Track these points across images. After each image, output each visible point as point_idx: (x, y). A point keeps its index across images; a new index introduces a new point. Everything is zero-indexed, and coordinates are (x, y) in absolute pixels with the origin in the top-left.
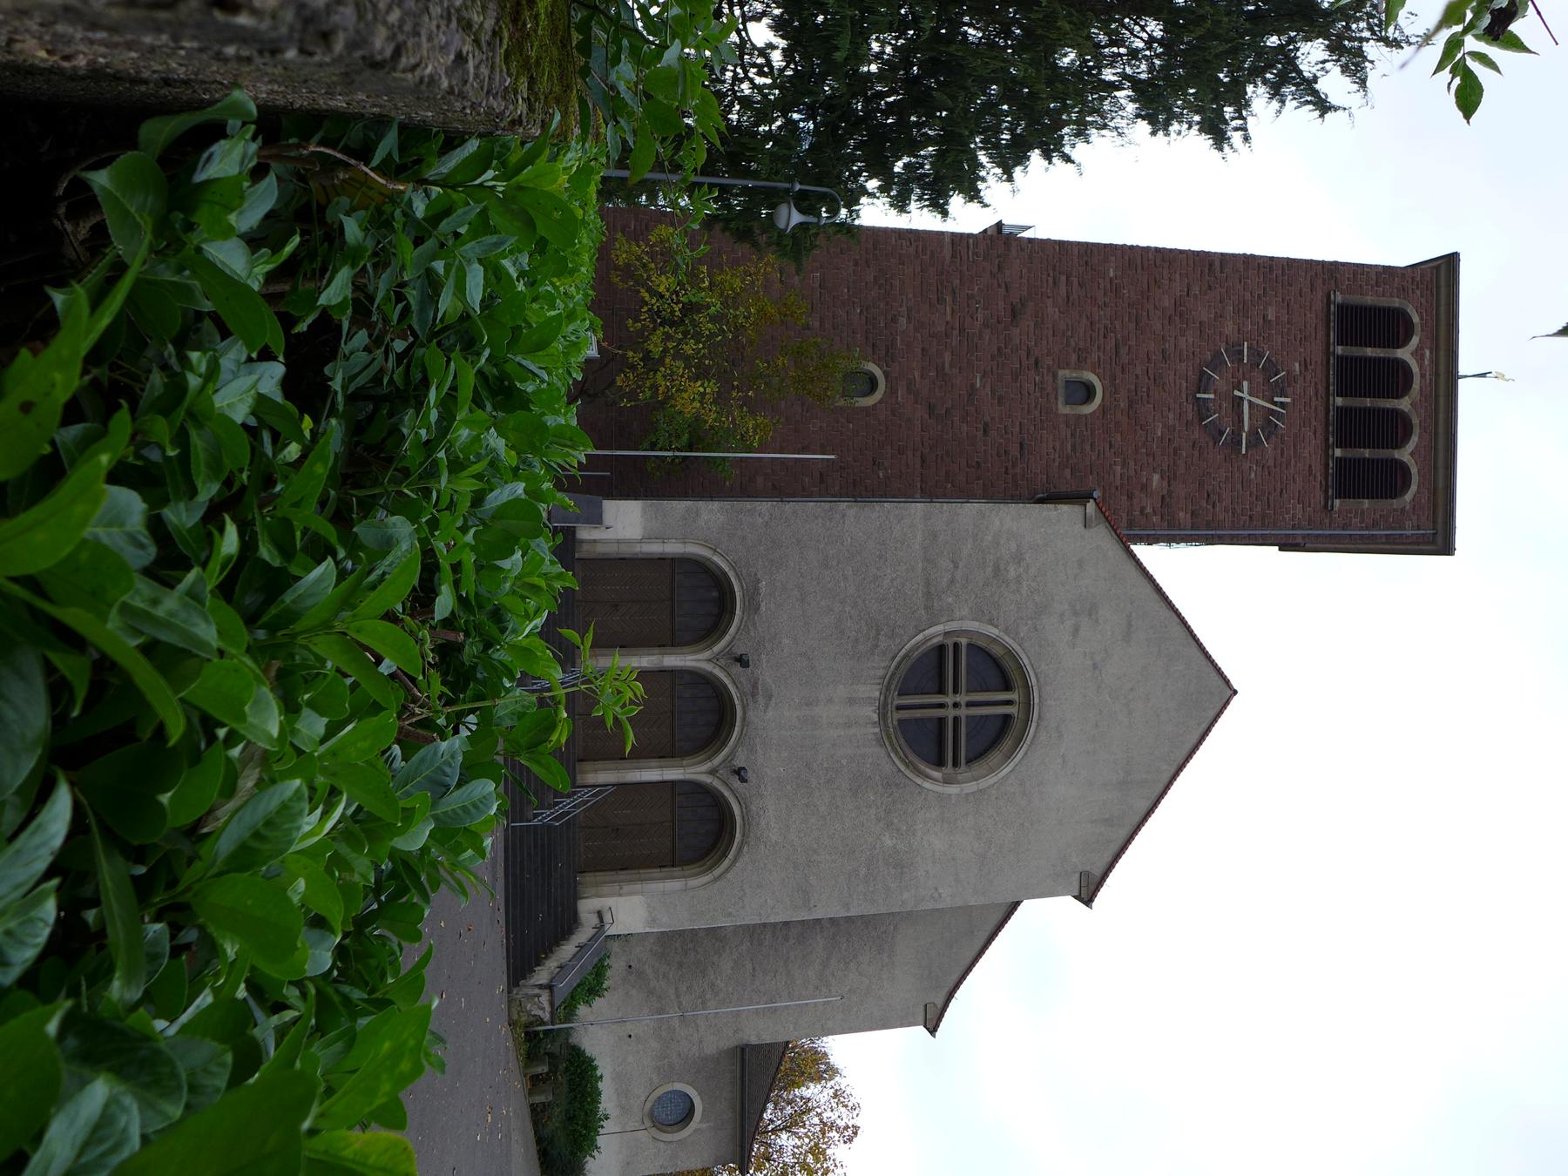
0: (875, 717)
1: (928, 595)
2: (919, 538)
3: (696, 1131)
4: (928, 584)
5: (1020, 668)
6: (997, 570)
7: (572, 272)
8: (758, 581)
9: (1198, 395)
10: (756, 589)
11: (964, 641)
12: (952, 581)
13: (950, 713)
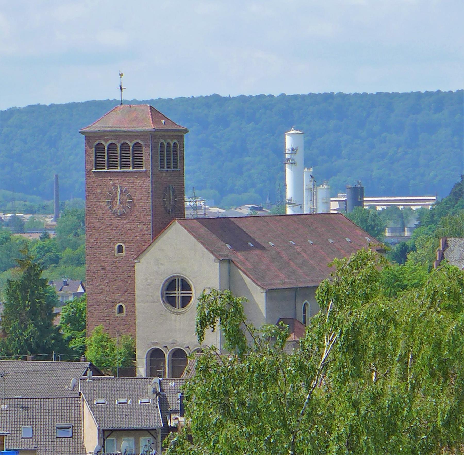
0: (179, 315)
1: (154, 302)
2: (142, 304)
3: (83, 392)
4: (152, 302)
5: (172, 277)
6: (149, 285)
7: (363, 280)
8: (151, 343)
9: (119, 215)
10: (153, 343)
11: (165, 292)
12: (151, 296)
13: (177, 295)
